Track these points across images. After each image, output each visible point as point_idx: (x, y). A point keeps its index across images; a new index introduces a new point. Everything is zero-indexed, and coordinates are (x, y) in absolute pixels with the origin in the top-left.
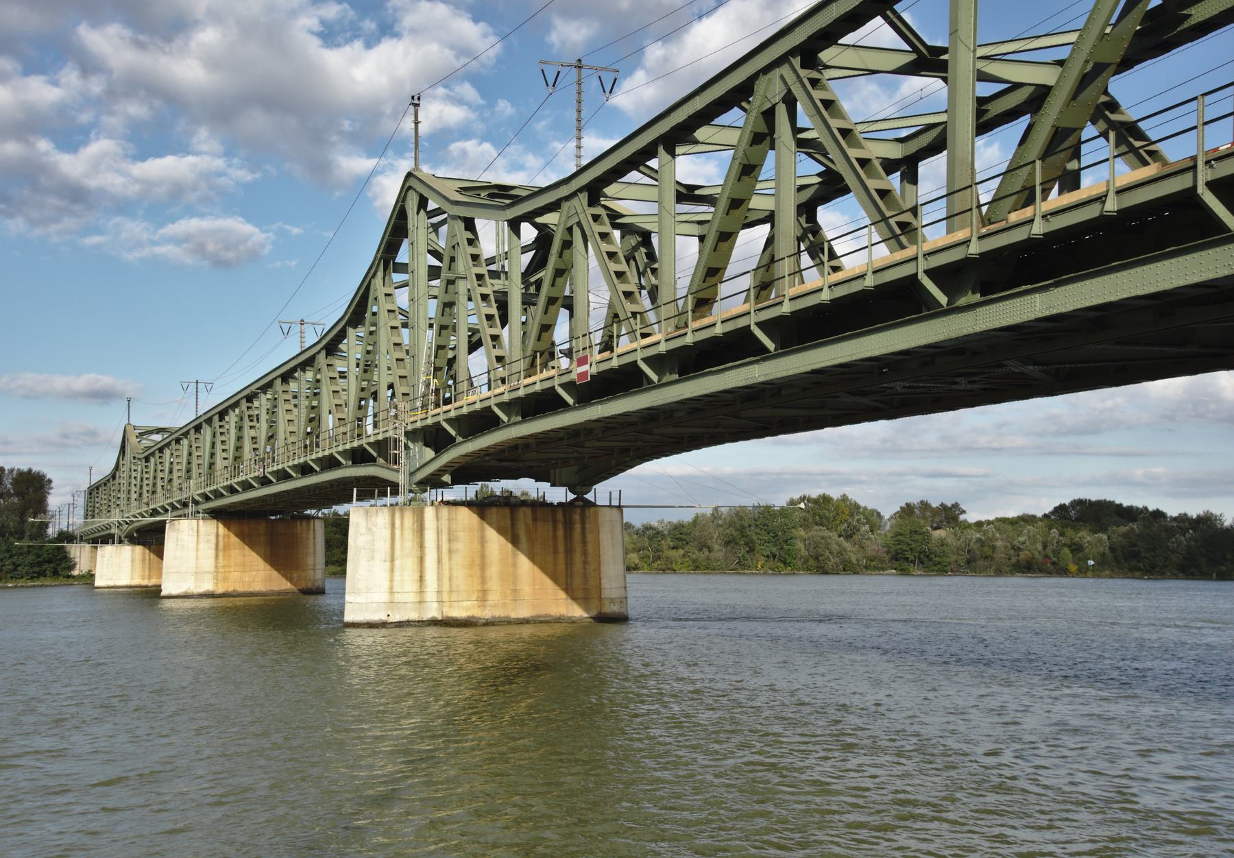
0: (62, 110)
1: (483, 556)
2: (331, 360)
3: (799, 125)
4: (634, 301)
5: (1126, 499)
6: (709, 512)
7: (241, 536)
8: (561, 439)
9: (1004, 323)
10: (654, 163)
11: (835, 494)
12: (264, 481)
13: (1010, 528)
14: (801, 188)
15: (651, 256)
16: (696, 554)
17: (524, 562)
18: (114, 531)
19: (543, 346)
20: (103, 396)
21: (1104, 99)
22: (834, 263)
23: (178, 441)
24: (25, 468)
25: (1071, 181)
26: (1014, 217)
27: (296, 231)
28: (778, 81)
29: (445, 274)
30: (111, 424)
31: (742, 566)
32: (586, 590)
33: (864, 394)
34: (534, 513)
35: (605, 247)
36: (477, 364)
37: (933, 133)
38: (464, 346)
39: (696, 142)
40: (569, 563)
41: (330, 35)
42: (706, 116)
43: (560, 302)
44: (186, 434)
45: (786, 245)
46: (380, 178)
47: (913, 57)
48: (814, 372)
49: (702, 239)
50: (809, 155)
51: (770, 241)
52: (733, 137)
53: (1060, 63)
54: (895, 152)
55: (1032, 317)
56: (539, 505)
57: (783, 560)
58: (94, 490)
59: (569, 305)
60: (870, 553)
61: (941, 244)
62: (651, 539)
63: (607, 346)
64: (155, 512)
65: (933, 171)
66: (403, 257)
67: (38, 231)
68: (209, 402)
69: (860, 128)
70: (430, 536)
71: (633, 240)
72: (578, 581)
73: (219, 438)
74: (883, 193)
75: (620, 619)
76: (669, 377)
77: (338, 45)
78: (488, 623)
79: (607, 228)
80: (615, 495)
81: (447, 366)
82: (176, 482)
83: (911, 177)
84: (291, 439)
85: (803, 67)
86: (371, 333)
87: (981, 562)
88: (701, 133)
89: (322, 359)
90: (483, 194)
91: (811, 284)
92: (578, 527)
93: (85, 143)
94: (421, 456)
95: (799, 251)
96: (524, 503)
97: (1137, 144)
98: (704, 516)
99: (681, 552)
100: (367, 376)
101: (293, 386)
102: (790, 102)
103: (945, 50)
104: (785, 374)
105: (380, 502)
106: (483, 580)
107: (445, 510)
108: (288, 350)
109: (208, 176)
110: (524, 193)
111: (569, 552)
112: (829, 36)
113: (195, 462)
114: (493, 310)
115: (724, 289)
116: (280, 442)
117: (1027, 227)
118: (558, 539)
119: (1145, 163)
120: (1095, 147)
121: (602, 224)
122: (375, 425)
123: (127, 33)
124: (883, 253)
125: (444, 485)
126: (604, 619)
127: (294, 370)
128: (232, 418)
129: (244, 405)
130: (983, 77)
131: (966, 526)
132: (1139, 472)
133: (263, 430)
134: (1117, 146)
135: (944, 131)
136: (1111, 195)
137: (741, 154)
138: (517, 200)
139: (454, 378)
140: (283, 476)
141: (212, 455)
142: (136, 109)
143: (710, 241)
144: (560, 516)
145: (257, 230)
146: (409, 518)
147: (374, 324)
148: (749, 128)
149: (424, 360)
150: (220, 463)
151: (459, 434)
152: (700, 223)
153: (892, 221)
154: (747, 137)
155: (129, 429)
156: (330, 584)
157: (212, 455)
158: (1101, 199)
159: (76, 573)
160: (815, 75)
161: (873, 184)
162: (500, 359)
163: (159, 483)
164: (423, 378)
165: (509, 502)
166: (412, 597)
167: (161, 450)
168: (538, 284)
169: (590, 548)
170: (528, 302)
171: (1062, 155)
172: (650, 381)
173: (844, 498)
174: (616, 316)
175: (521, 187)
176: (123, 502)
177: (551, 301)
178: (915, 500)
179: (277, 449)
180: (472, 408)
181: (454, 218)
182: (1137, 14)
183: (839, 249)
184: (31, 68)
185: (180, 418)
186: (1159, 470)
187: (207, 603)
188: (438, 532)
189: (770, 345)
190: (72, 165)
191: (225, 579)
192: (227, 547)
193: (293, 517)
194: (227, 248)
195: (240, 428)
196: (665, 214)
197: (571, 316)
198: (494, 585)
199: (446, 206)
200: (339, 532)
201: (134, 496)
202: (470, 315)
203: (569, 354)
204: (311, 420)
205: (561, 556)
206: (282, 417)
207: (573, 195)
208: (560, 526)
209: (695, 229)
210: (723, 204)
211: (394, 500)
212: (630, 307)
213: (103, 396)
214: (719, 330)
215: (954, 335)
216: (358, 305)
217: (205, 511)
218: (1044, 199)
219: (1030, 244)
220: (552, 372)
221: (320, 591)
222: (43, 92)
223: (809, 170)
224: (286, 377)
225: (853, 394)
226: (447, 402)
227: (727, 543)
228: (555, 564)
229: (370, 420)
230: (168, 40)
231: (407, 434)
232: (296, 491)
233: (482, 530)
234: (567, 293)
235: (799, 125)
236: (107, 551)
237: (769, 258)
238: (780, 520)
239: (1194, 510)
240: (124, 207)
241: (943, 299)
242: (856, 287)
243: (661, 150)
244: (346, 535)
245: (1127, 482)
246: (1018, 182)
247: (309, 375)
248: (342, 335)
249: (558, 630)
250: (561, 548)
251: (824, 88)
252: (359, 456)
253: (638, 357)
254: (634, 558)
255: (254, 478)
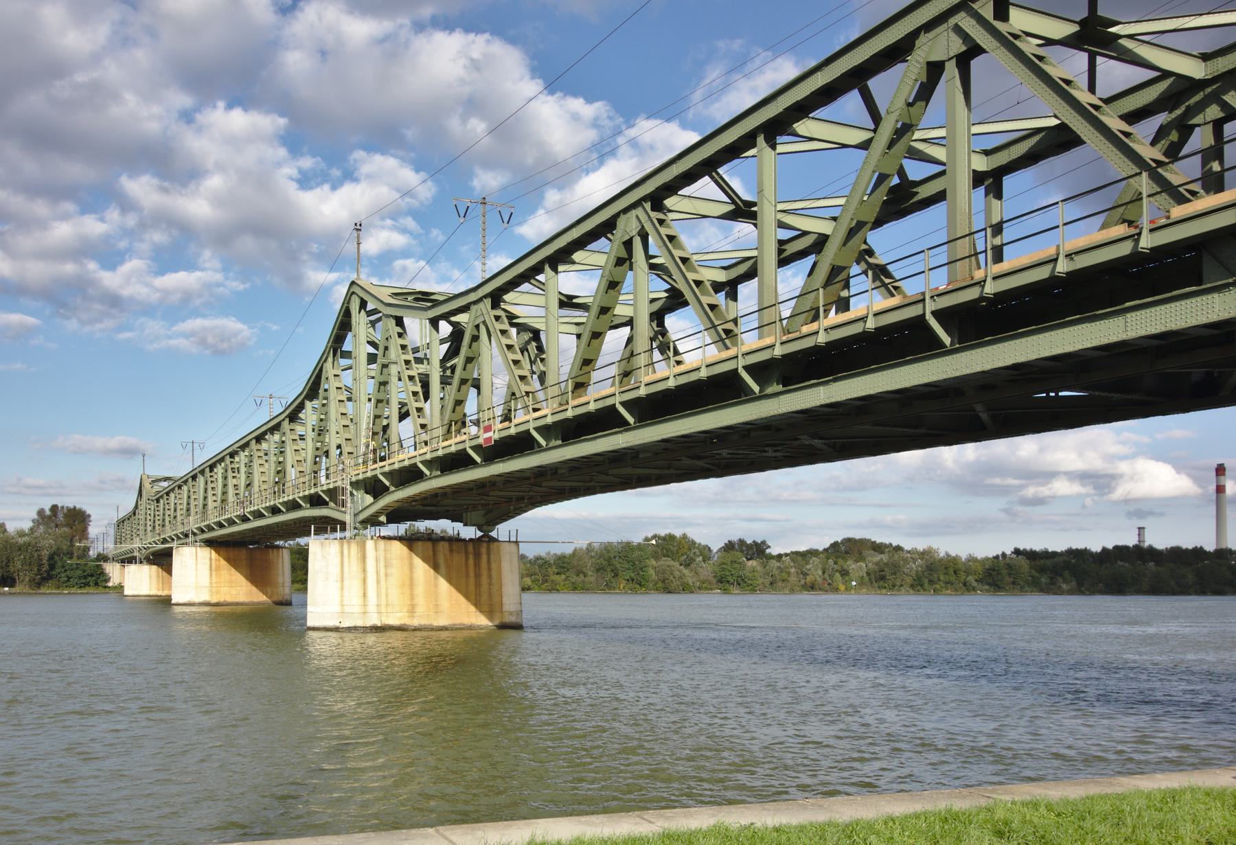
0: (107, 239)
1: (412, 579)
2: (293, 426)
3: (651, 253)
4: (527, 384)
5: (879, 538)
6: (585, 547)
7: (228, 560)
8: (471, 489)
9: (799, 408)
10: (541, 277)
11: (678, 533)
12: (245, 519)
13: (800, 558)
14: (653, 301)
15: (540, 349)
16: (574, 578)
17: (443, 584)
18: (136, 554)
19: (457, 416)
20: (128, 452)
21: (864, 247)
22: (678, 358)
23: (180, 487)
24: (72, 506)
25: (843, 305)
26: (806, 329)
27: (275, 327)
28: (634, 220)
29: (380, 360)
30: (132, 472)
31: (608, 588)
32: (491, 605)
33: (699, 458)
34: (450, 546)
35: (505, 341)
36: (406, 430)
37: (750, 263)
38: (395, 416)
39: (574, 263)
40: (478, 585)
41: (306, 181)
42: (581, 243)
43: (470, 383)
44: (186, 482)
45: (642, 343)
46: (338, 287)
47: (732, 207)
48: (664, 441)
49: (579, 336)
50: (658, 275)
51: (630, 340)
52: (601, 260)
53: (835, 219)
54: (721, 277)
55: (818, 403)
56: (455, 540)
57: (639, 583)
58: (121, 523)
59: (477, 385)
60: (702, 578)
61: (755, 347)
62: (540, 566)
63: (507, 418)
64: (164, 541)
65: (747, 290)
66: (347, 346)
67: (87, 329)
68: (203, 457)
69: (695, 257)
70: (371, 562)
71: (527, 336)
72: (485, 597)
73: (210, 486)
74: (713, 307)
75: (518, 627)
76: (554, 443)
77: (311, 188)
78: (416, 629)
79: (506, 326)
80: (513, 534)
81: (382, 431)
82: (179, 518)
83: (733, 296)
84: (264, 487)
85: (653, 210)
86: (324, 405)
87: (780, 584)
88: (578, 256)
89: (286, 425)
90: (410, 298)
91: (660, 374)
92: (484, 557)
93: (122, 262)
94: (363, 501)
95: (652, 349)
96: (443, 539)
97: (887, 281)
98: (581, 549)
99: (563, 577)
100: (320, 438)
101: (264, 445)
102: (644, 236)
103: (755, 204)
104: (641, 442)
105: (332, 536)
106: (412, 598)
107: (382, 543)
108: (260, 418)
109: (208, 286)
110: (441, 298)
111: (478, 576)
112: (671, 188)
113: (193, 503)
114: (418, 388)
115: (595, 376)
116: (256, 489)
117: (814, 337)
118: (467, 565)
119: (893, 295)
120: (860, 282)
121: (503, 323)
122: (327, 477)
123: (155, 181)
124: (713, 353)
125: (381, 524)
126: (503, 627)
127: (265, 433)
128: (219, 470)
129: (228, 459)
130: (782, 225)
131: (771, 557)
132: (889, 518)
133: (242, 482)
134: (874, 281)
135: (756, 263)
136: (870, 316)
137: (607, 273)
138: (436, 303)
139: (388, 441)
140: (258, 515)
141: (205, 498)
142: (158, 237)
143: (585, 338)
144: (471, 548)
145: (244, 327)
146: (354, 548)
147: (326, 398)
148: (613, 254)
149: (364, 426)
150: (211, 505)
151: (392, 484)
152: (577, 324)
153: (720, 328)
154: (613, 261)
155: (145, 477)
156: (295, 599)
157: (205, 498)
158: (863, 319)
159: (110, 584)
160: (661, 216)
161: (706, 300)
162: (423, 426)
163: (167, 519)
164: (364, 441)
165: (431, 538)
166: (358, 609)
167: (168, 494)
168: (453, 368)
169: (494, 573)
170: (445, 382)
171: (837, 286)
172: (540, 445)
173: (685, 536)
174: (514, 394)
175: (439, 294)
176: (141, 533)
177: (463, 382)
178: (735, 539)
179: (254, 494)
180: (402, 465)
181: (388, 316)
182: (884, 189)
183: (681, 349)
184: (86, 209)
185: (181, 470)
186: (901, 517)
187: (207, 609)
188: (377, 560)
189: (631, 420)
190: (110, 280)
191: (218, 592)
192: (218, 568)
193: (267, 547)
194: (222, 341)
195: (226, 478)
196: (550, 317)
197: (479, 394)
198: (421, 601)
199: (381, 307)
200: (301, 560)
201: (149, 528)
202: (400, 391)
203: (477, 423)
204: (278, 472)
205: (472, 579)
206: (256, 470)
207: (480, 300)
208: (471, 557)
209: (574, 329)
210: (595, 310)
211: (342, 535)
212: (524, 388)
213: (128, 452)
214: (592, 407)
215: (764, 416)
216: (314, 383)
217: (201, 541)
218: (826, 317)
219: (816, 349)
220: (464, 437)
221: (288, 603)
222: (94, 227)
223: (659, 289)
224: (259, 439)
225: (879, 425)
226: (383, 459)
227: (598, 570)
228: (467, 585)
229: (323, 473)
230: (184, 185)
231: (351, 484)
232: (268, 526)
233: (411, 559)
234: (475, 376)
235: (651, 253)
236: (132, 569)
237: (630, 354)
238: (637, 553)
239: (920, 544)
240: (148, 310)
241: (756, 388)
242: (693, 377)
243: (547, 267)
244: (307, 561)
245: (879, 526)
246: (808, 303)
247: (277, 437)
248: (301, 407)
249: (466, 633)
250: (472, 574)
251: (668, 227)
252: (316, 501)
253: (531, 426)
254: (528, 581)
255: (237, 516)
